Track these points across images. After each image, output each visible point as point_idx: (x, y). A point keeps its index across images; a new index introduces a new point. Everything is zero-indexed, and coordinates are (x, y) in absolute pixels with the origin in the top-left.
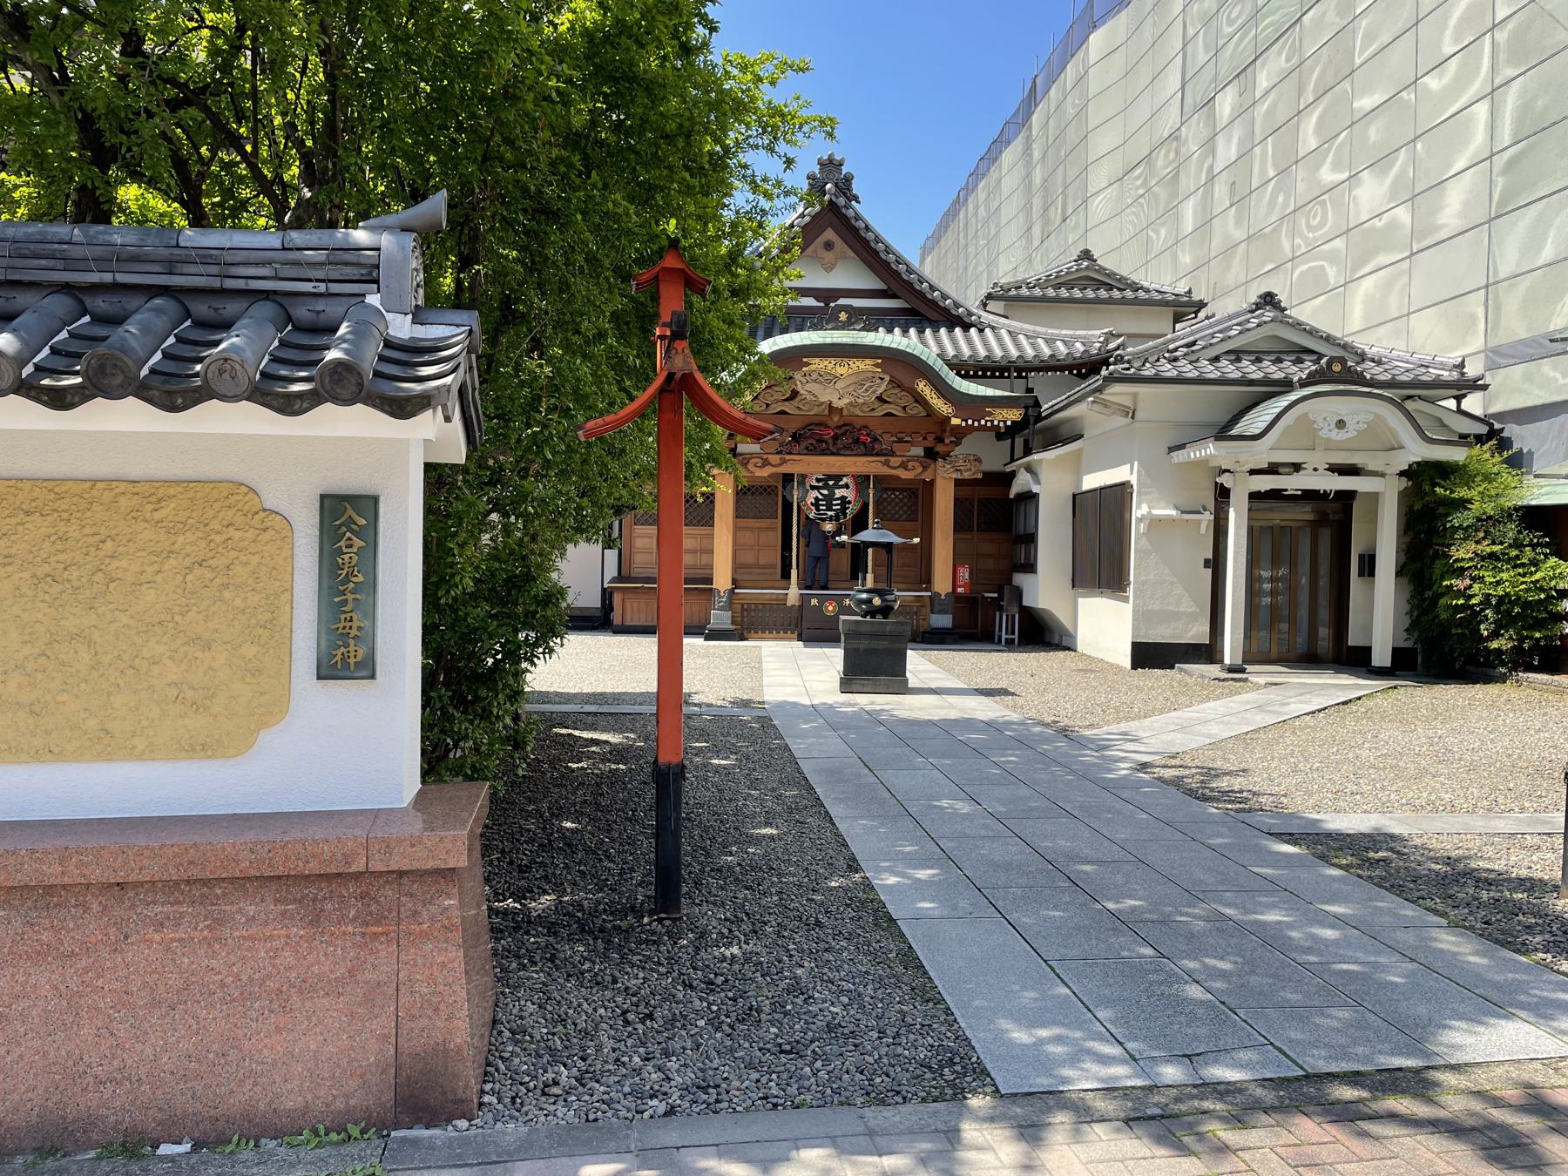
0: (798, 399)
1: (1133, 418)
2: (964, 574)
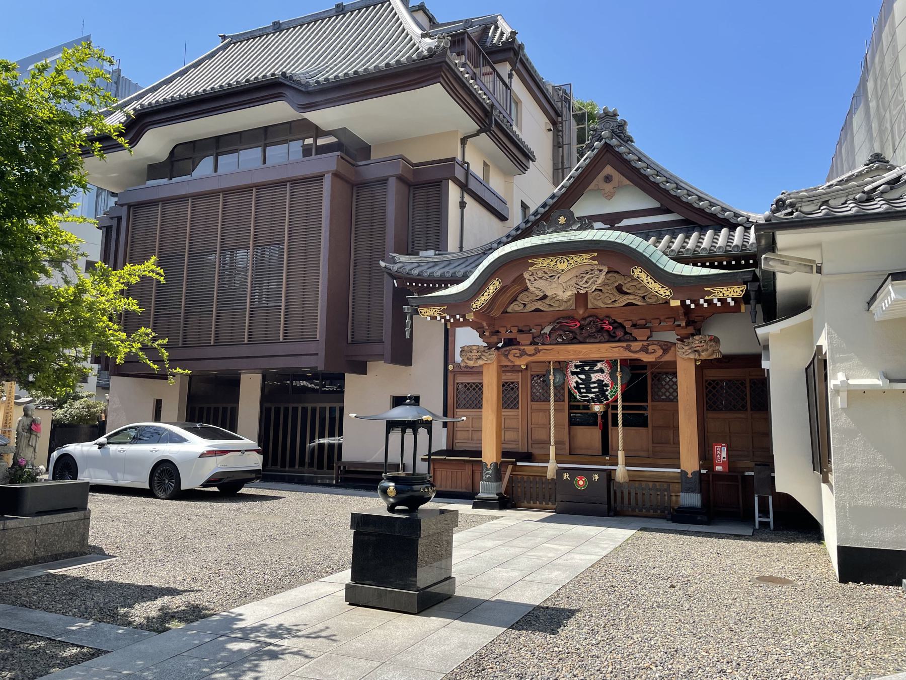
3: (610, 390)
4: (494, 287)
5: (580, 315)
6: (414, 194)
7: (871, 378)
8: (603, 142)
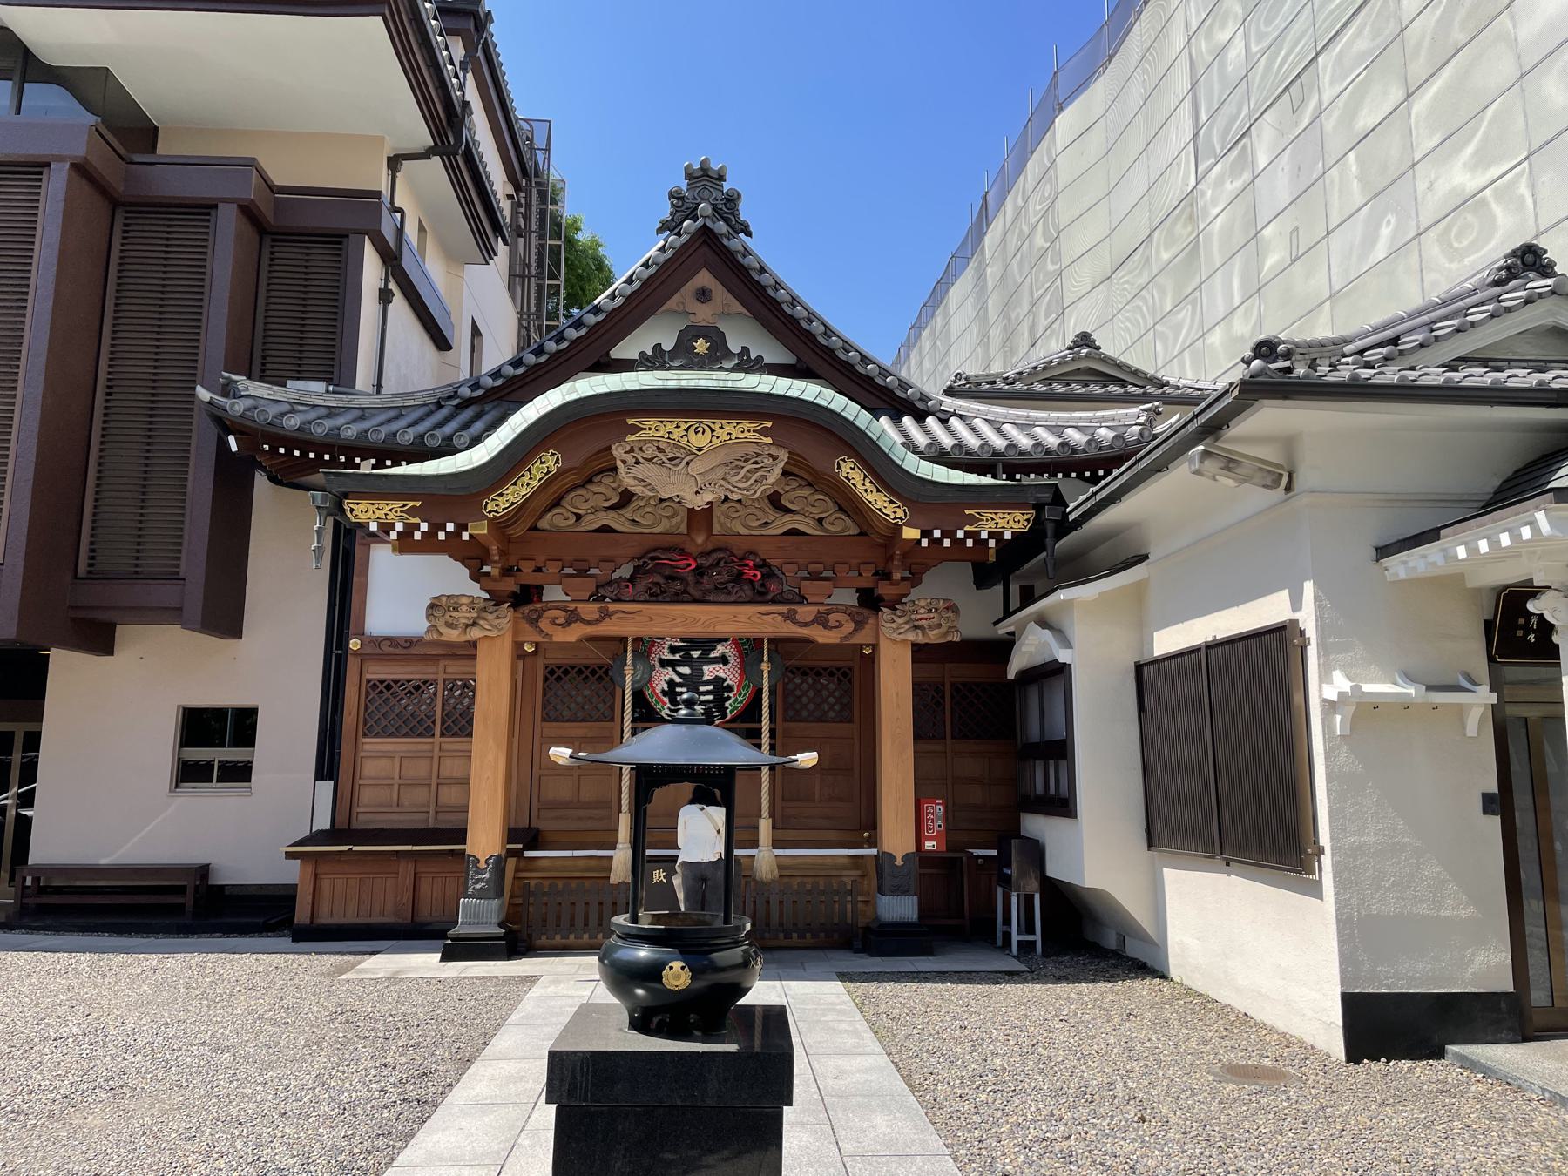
0: (634, 505)
1: (1288, 488)
2: (935, 811)
3: (733, 698)
4: (547, 464)
5: (697, 546)
6: (272, 253)
7: (1384, 682)
8: (700, 222)
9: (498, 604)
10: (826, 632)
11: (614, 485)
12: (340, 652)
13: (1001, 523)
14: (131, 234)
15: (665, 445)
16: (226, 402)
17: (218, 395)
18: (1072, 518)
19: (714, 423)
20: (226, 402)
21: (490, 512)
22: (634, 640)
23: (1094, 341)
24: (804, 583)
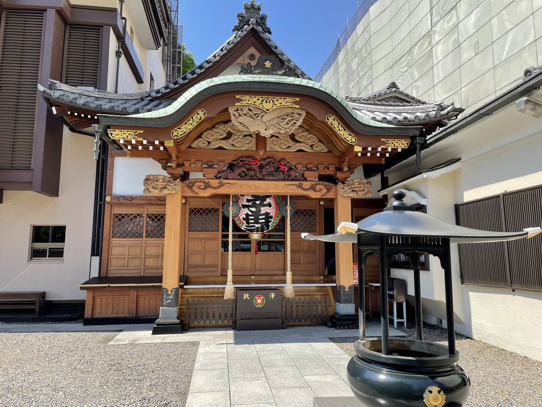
0: (232, 138)
4: (200, 115)
5: (260, 156)
8: (251, 26)
9: (175, 179)
10: (315, 193)
11: (224, 129)
12: (101, 203)
13: (397, 145)
14: (9, 24)
15: (252, 108)
16: (51, 92)
17: (47, 88)
18: (428, 142)
19: (274, 98)
20: (51, 92)
21: (175, 136)
22: (233, 196)
23: (397, 86)
24: (306, 172)
